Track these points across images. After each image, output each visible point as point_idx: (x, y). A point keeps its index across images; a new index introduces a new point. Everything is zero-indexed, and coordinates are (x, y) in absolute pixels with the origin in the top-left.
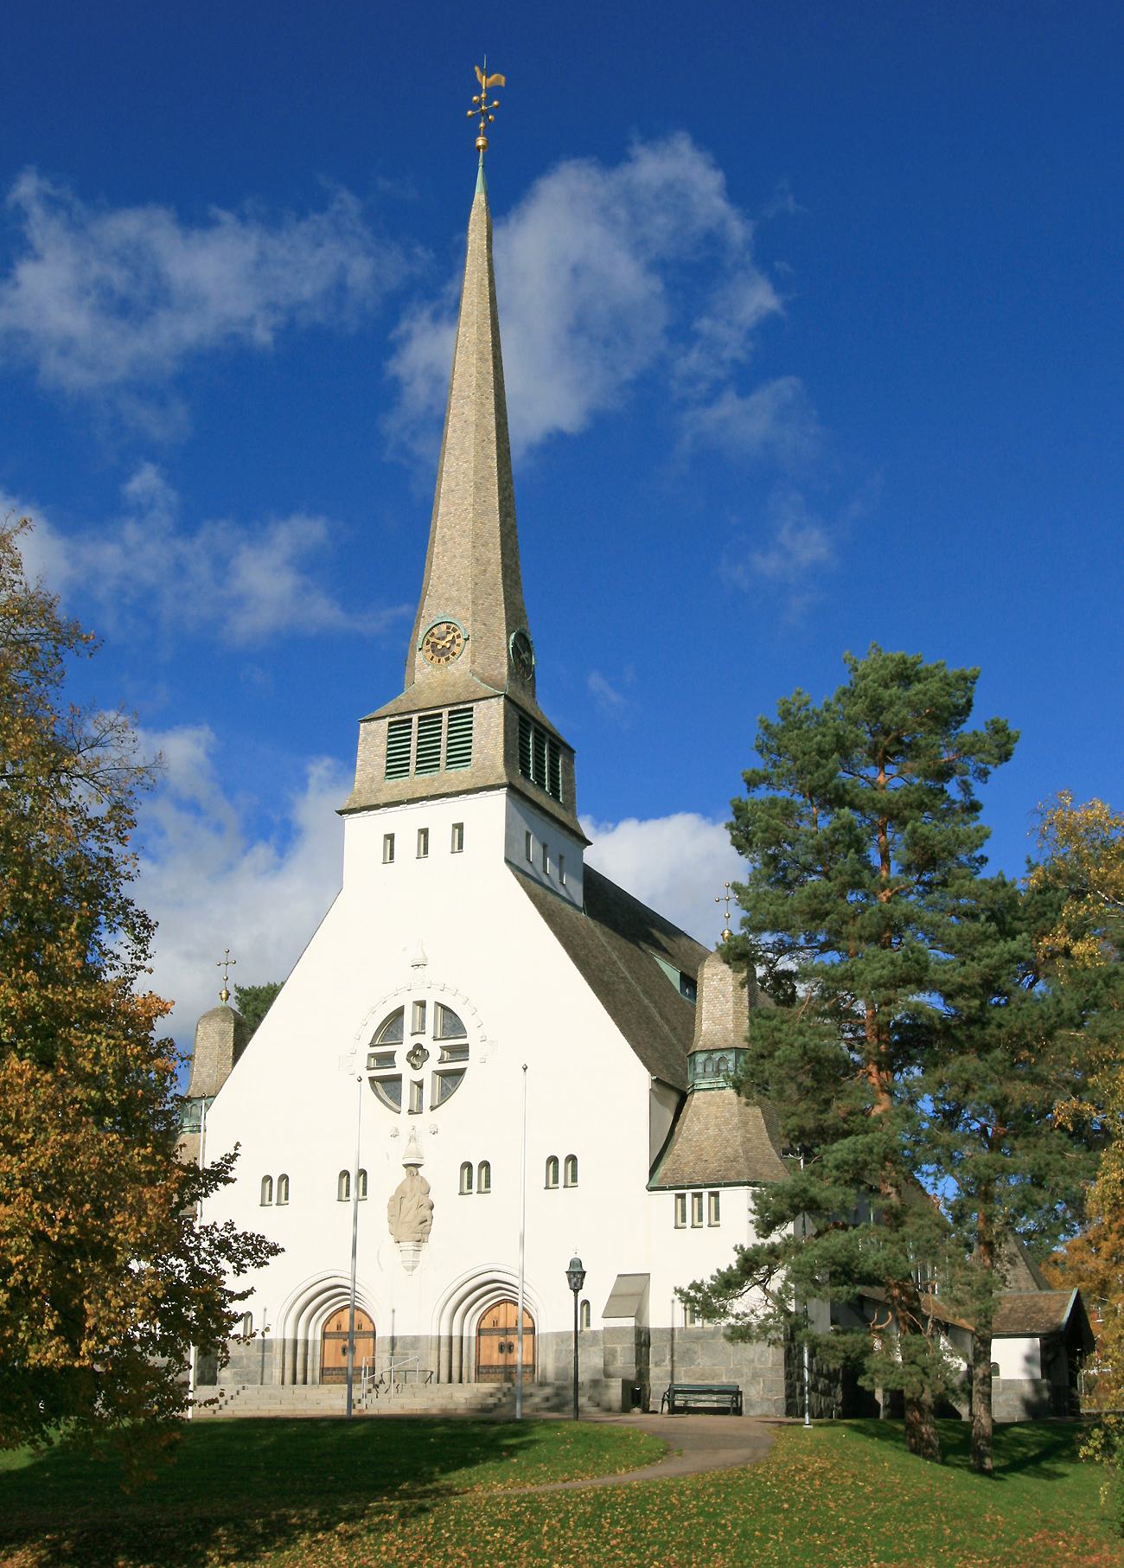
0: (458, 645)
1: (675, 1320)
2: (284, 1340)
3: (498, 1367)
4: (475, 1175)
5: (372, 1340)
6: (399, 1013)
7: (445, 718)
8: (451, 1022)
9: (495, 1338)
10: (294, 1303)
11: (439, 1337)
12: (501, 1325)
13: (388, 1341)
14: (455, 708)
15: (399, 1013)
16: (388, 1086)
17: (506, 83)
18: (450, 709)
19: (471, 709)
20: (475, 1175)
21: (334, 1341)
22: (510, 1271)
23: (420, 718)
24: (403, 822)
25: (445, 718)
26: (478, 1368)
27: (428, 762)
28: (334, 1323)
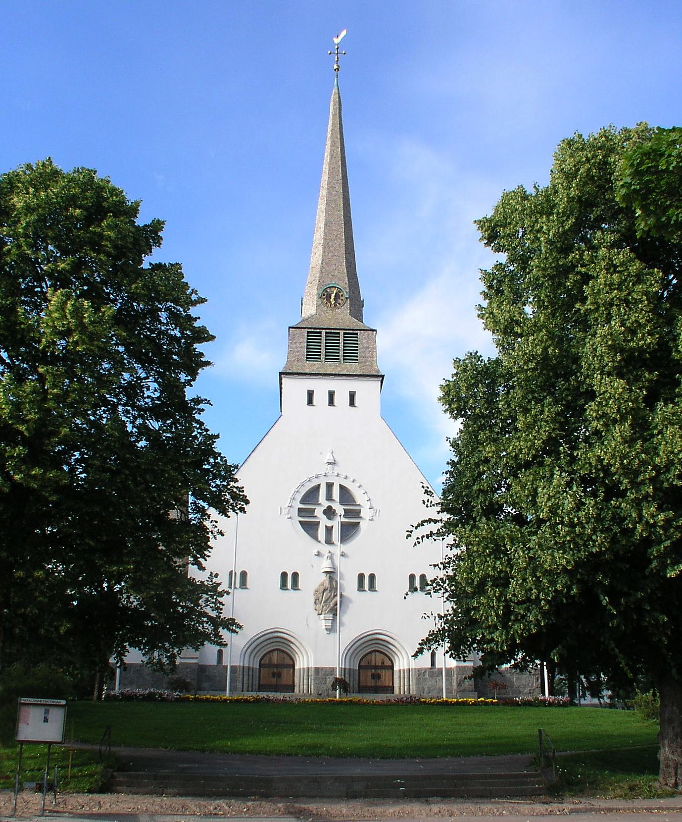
0: (342, 300)
1: (245, 663)
2: (244, 667)
3: (372, 687)
4: (367, 582)
5: (291, 670)
6: (318, 487)
7: (342, 335)
8: (346, 495)
9: (369, 671)
10: (250, 645)
11: (244, 667)
12: (373, 664)
13: (398, 671)
14: (347, 332)
15: (318, 487)
16: (310, 528)
17: (343, 30)
18: (309, 330)
19: (357, 334)
20: (367, 582)
21: (266, 669)
22: (288, 632)
23: (345, 334)
24: (321, 387)
25: (342, 335)
26: (359, 687)
27: (331, 356)
28: (267, 658)
